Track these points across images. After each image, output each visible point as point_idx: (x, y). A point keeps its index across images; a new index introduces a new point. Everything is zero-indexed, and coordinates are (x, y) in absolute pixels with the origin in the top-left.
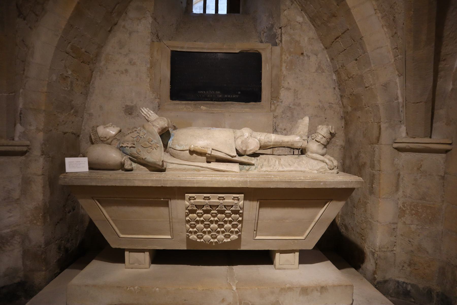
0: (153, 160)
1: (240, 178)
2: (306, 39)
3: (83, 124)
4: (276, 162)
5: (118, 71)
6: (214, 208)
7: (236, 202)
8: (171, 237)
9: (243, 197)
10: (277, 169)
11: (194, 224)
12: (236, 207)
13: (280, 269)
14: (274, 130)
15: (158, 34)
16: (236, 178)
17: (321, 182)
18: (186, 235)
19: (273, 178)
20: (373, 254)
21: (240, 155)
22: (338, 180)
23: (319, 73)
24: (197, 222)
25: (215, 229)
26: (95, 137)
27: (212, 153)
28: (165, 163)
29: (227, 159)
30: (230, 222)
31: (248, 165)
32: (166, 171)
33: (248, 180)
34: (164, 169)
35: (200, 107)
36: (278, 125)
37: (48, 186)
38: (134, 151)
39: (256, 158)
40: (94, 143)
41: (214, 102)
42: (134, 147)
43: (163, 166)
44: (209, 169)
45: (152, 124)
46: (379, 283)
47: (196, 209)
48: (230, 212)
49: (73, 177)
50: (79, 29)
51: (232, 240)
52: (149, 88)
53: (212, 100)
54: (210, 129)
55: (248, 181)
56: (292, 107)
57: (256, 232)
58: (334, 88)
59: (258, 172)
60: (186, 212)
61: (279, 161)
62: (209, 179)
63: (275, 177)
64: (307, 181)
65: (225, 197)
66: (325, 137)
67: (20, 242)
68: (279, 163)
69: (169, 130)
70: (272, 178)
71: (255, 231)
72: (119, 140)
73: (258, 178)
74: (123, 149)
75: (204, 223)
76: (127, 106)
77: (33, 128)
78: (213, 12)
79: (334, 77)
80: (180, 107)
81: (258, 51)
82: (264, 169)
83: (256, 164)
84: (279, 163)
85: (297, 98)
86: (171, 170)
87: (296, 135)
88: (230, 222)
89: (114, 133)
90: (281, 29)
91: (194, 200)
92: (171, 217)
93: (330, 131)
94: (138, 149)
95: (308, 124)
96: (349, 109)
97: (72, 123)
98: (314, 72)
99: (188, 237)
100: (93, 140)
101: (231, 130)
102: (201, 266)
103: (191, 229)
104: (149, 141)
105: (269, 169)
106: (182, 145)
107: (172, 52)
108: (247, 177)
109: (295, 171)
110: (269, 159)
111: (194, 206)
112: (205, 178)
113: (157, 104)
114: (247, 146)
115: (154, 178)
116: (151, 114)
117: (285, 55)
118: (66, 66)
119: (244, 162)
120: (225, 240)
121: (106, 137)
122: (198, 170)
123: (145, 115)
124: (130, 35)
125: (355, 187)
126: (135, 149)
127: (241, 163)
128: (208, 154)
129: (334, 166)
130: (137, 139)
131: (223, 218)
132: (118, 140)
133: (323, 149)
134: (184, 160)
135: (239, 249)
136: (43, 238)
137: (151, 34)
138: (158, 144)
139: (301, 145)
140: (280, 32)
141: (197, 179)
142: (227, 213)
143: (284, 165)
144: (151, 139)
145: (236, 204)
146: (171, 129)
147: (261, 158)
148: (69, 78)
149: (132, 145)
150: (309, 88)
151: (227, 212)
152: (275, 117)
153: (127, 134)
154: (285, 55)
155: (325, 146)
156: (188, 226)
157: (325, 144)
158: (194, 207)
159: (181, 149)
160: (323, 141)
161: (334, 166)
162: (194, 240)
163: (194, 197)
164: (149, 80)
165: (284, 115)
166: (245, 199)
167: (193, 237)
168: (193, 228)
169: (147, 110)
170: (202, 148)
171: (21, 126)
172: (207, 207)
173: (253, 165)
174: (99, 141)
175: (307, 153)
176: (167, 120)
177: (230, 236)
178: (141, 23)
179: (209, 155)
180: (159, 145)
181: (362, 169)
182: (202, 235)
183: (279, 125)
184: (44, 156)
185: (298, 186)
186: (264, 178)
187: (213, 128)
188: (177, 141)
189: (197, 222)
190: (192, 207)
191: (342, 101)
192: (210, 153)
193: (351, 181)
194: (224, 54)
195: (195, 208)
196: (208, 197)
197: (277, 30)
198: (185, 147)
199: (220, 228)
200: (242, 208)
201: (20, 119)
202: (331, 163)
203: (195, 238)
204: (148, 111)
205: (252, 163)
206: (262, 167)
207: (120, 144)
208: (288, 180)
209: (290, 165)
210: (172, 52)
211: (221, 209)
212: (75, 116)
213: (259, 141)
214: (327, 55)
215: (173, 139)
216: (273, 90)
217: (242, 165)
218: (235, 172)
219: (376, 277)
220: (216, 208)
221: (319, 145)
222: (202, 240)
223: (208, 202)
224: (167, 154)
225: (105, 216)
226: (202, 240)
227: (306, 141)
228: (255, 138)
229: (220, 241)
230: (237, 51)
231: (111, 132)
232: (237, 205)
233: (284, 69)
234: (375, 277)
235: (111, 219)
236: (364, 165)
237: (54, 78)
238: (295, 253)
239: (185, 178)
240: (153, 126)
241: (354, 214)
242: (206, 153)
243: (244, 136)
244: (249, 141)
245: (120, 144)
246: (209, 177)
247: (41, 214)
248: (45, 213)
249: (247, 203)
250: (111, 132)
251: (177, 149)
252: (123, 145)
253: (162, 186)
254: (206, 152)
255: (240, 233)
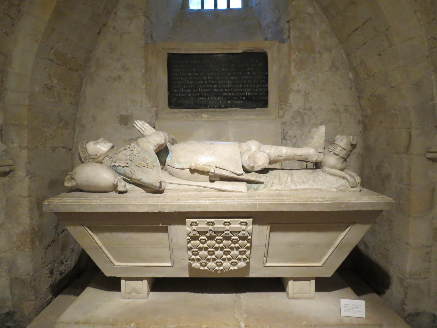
0: (149, 181)
1: (248, 201)
2: (318, 34)
3: (75, 137)
4: (288, 178)
5: (110, 77)
6: (219, 234)
7: (244, 227)
8: (172, 265)
9: (252, 221)
10: (289, 188)
11: (197, 252)
12: (244, 233)
13: (293, 298)
14: (282, 138)
15: (152, 35)
16: (243, 201)
17: (342, 204)
18: (188, 263)
19: (286, 200)
20: (402, 281)
21: (247, 171)
22: (362, 202)
23: (333, 72)
24: (200, 249)
25: (221, 256)
26: (84, 155)
27: (215, 172)
28: (163, 184)
29: (231, 178)
30: (237, 248)
31: (256, 184)
32: (164, 193)
33: (257, 203)
34: (162, 190)
35: (201, 115)
36: (287, 133)
37: (36, 208)
38: (128, 171)
39: (265, 174)
40: (83, 161)
41: (216, 109)
42: (128, 167)
43: (161, 187)
44: (213, 190)
45: (147, 140)
46: (410, 315)
47: (199, 235)
48: (237, 238)
49: (58, 203)
50: (62, 33)
51: (239, 267)
52: (145, 96)
53: (214, 108)
54: (212, 143)
55: (257, 204)
56: (303, 112)
57: (267, 258)
58: (351, 89)
59: (268, 191)
60: (187, 239)
61: (291, 178)
62: (212, 202)
63: (288, 199)
64: (326, 203)
65: (231, 223)
66: (344, 150)
67: (7, 270)
68: (292, 180)
69: (167, 146)
70: (285, 200)
71: (265, 257)
72: (111, 157)
73: (269, 201)
74: (115, 169)
75: (207, 250)
76: (121, 116)
77: (16, 145)
78: (212, 7)
79: (351, 75)
80: (179, 116)
81: (264, 50)
82: (275, 187)
83: (266, 182)
84: (291, 181)
85: (308, 101)
86: (170, 190)
87: (310, 147)
88: (237, 248)
89: (106, 149)
90: (289, 23)
91: (196, 226)
92: (171, 244)
93: (351, 142)
94: (132, 168)
95: (324, 135)
96: (369, 112)
97: (62, 137)
98: (327, 71)
99: (190, 265)
100: (82, 158)
101: (236, 143)
102: (205, 294)
103: (193, 257)
104: (145, 160)
105: (280, 187)
106: (181, 163)
107: (169, 54)
108: (256, 199)
109: (310, 189)
110: (280, 175)
111: (197, 232)
112: (208, 202)
113: (155, 112)
114: (254, 161)
115: (150, 202)
116: (146, 128)
117: (294, 52)
118: (50, 74)
119: (252, 180)
120: (232, 268)
121: (96, 155)
122: (200, 190)
123: (139, 128)
124: (121, 37)
125: (384, 209)
126: (129, 168)
127: (249, 182)
128: (211, 173)
129: (357, 183)
130: (130, 157)
131: (229, 245)
132: (110, 158)
133: (342, 163)
134: (183, 179)
135: (247, 277)
136: (32, 264)
137: (145, 35)
138: (154, 163)
139: (316, 159)
140: (288, 26)
141: (199, 203)
142: (233, 240)
143: (297, 182)
144: (146, 158)
145: (244, 230)
146: (169, 144)
147: (271, 174)
148: (55, 87)
149: (126, 164)
150: (321, 90)
151: (233, 238)
152: (283, 124)
153: (120, 151)
154: (294, 52)
155: (345, 160)
156: (190, 253)
157: (345, 157)
158: (196, 233)
159: (181, 168)
160: (343, 154)
161: (357, 183)
162: (197, 268)
163: (196, 223)
164: (145, 87)
165: (293, 121)
166: (254, 223)
167: (196, 265)
168: (195, 255)
169: (142, 123)
170: (204, 167)
171: (3, 143)
172: (210, 233)
173: (263, 183)
174: (89, 159)
175: (323, 167)
176: (163, 135)
177: (237, 263)
178: (133, 22)
179: (213, 174)
180: (155, 164)
181: (386, 181)
182: (205, 263)
183: (288, 132)
184: (29, 176)
185: (316, 209)
186: (276, 199)
187: (216, 142)
188: (176, 158)
189: (200, 249)
190: (194, 234)
191: (359, 103)
192: (213, 172)
193: (379, 202)
194: (226, 55)
195: (198, 235)
196: (212, 223)
197: (284, 24)
198: (185, 164)
199: (226, 255)
200: (251, 234)
201: (1, 136)
202: (353, 180)
203: (198, 266)
204: (143, 124)
205: (261, 181)
206: (272, 186)
207: (112, 162)
208: (303, 202)
209: (304, 182)
210: (169, 54)
211: (227, 235)
212: (65, 128)
213: (269, 155)
214: (342, 51)
215: (171, 156)
216: (281, 94)
217: (249, 183)
218: (243, 192)
219: (407, 309)
220: (221, 234)
221: (338, 159)
222: (206, 268)
223: (213, 227)
224: (165, 172)
225: (97, 243)
226: (206, 268)
227: (323, 154)
228: (264, 152)
229: (226, 269)
230: (240, 51)
231: (102, 148)
232: (245, 231)
233: (293, 69)
234: (404, 309)
235: (105, 247)
236: (388, 176)
237: (37, 89)
238: (310, 281)
239: (186, 201)
240: (149, 142)
241: (376, 231)
242: (209, 172)
243: (251, 150)
244: (257, 156)
245: (112, 162)
246: (212, 200)
247: (29, 240)
248: (32, 238)
249: (257, 227)
250: (102, 148)
251: (176, 167)
252: (116, 165)
253: (160, 211)
254: (209, 171)
255: (248, 261)
